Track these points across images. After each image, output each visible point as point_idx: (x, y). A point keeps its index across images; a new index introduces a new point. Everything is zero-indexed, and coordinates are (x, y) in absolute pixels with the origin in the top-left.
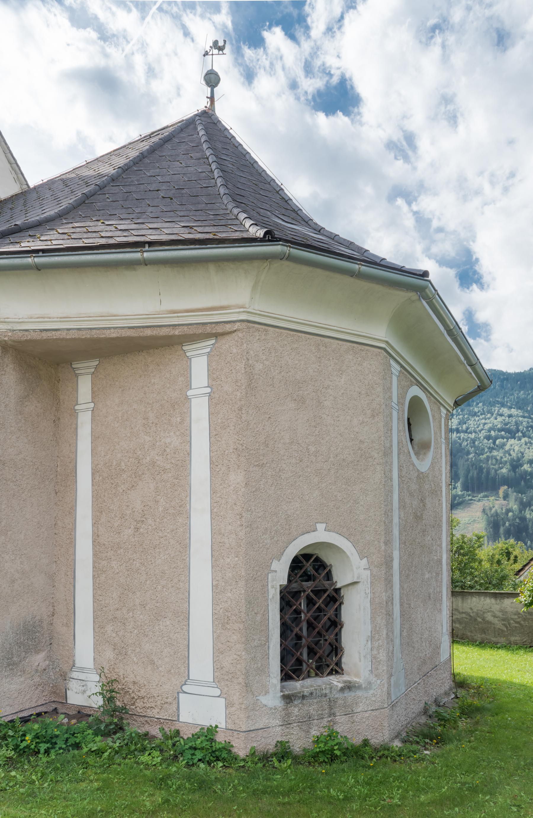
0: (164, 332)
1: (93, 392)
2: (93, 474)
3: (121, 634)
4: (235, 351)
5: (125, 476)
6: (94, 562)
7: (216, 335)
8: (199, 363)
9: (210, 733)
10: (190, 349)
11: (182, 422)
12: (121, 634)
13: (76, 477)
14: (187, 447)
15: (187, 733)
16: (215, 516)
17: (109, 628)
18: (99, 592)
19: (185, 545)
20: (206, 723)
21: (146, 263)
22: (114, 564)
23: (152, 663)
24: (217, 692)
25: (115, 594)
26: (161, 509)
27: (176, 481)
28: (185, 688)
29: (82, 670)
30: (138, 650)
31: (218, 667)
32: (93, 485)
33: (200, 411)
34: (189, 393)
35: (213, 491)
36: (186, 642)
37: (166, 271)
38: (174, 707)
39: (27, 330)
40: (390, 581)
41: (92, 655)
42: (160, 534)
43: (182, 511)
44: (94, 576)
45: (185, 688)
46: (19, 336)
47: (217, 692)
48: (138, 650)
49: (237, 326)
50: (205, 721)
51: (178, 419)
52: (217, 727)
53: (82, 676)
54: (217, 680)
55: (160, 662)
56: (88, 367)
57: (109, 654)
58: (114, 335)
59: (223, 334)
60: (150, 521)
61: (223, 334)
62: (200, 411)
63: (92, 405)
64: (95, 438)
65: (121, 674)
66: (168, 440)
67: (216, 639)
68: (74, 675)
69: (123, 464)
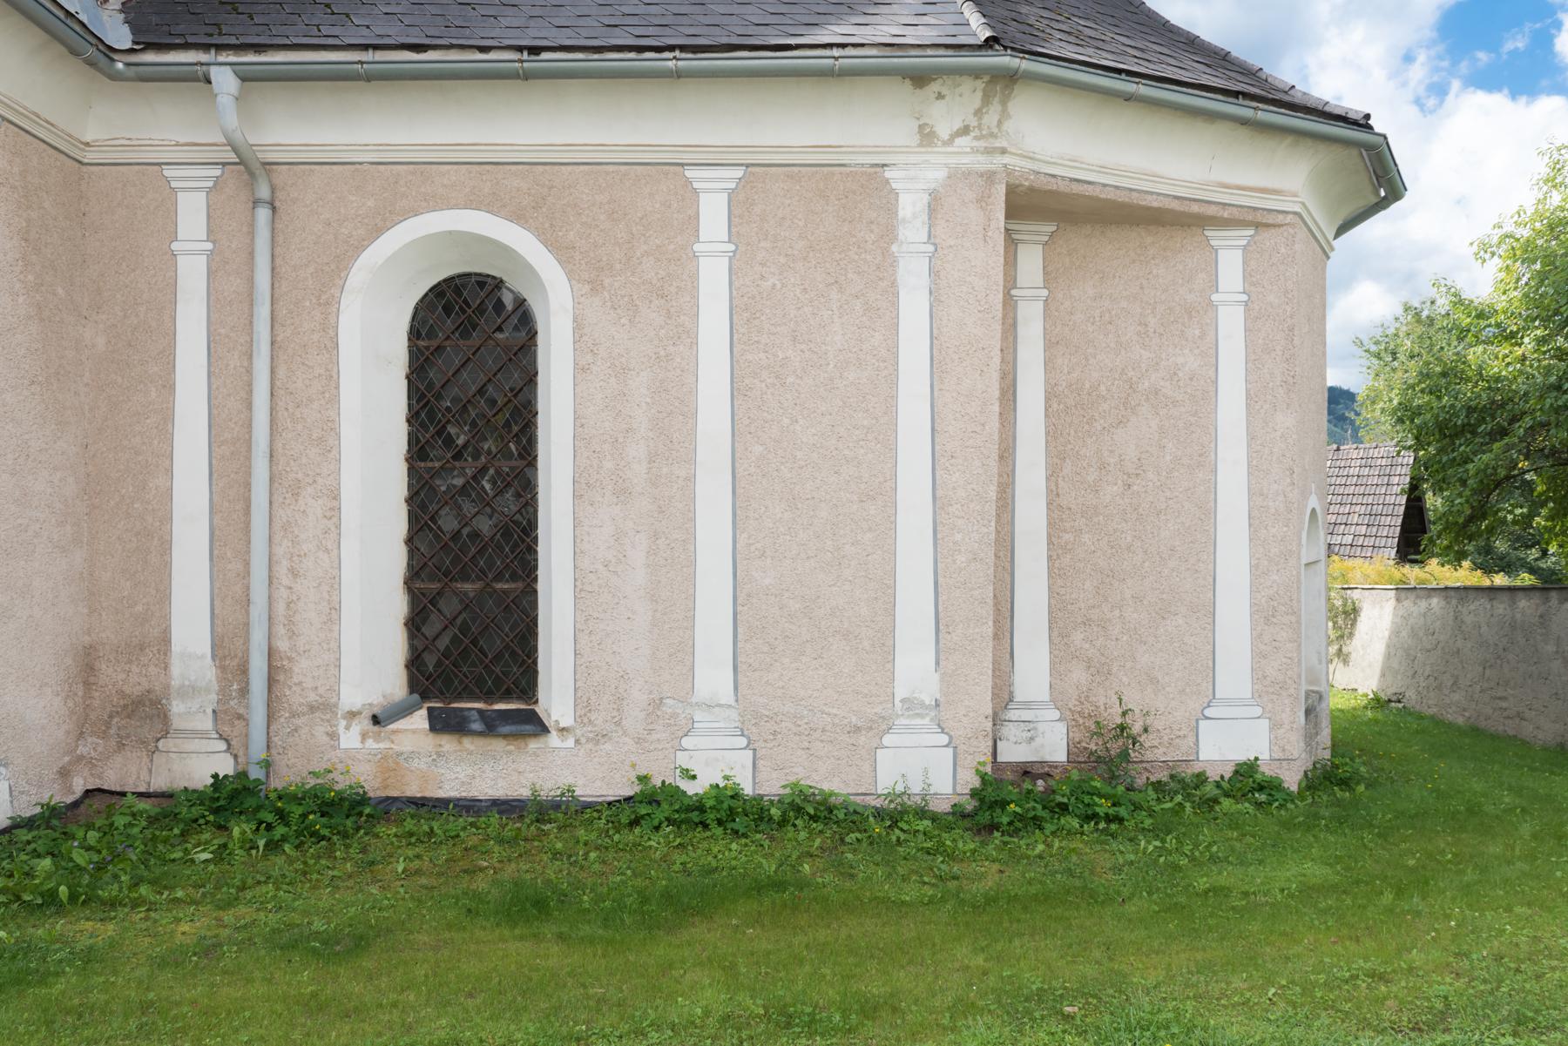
0: (1195, 208)
1: (1046, 273)
2: (1047, 400)
3: (1098, 644)
4: (1283, 250)
5: (1106, 406)
6: (1049, 536)
7: (1258, 225)
8: (1230, 257)
9: (1246, 770)
10: (1216, 237)
11: (1202, 336)
12: (1098, 644)
13: (1015, 401)
14: (1212, 373)
15: (1213, 775)
16: (1255, 469)
17: (1078, 637)
18: (1060, 582)
19: (1208, 512)
20: (1243, 756)
21: (1129, 98)
22: (1086, 538)
23: (1154, 681)
24: (1057, 714)
25: (1088, 583)
26: (1168, 458)
27: (1193, 420)
28: (1207, 712)
29: (1027, 705)
30: (1129, 665)
31: (1258, 676)
32: (1046, 416)
33: (1231, 324)
34: (1215, 297)
35: (1252, 437)
36: (1210, 647)
37: (1243, 132)
38: (1191, 740)
39: (1054, 176)
40: (527, 503)
41: (1046, 679)
42: (1168, 494)
43: (1204, 461)
44: (1050, 558)
45: (1207, 712)
46: (1043, 183)
47: (1258, 711)
48: (1129, 665)
49: (1289, 218)
50: (1241, 754)
51: (1197, 332)
52: (1257, 759)
53: (1026, 715)
54: (1257, 695)
55: (1167, 679)
56: (1038, 233)
57: (1079, 675)
58: (1155, 204)
59: (1268, 226)
60: (1150, 475)
61: (1268, 226)
62: (1231, 324)
63: (1045, 292)
64: (1050, 344)
65: (1101, 703)
66: (1180, 360)
67: (1257, 638)
68: (1013, 715)
69: (1103, 388)
